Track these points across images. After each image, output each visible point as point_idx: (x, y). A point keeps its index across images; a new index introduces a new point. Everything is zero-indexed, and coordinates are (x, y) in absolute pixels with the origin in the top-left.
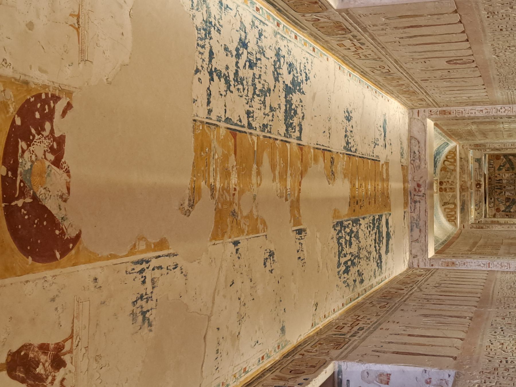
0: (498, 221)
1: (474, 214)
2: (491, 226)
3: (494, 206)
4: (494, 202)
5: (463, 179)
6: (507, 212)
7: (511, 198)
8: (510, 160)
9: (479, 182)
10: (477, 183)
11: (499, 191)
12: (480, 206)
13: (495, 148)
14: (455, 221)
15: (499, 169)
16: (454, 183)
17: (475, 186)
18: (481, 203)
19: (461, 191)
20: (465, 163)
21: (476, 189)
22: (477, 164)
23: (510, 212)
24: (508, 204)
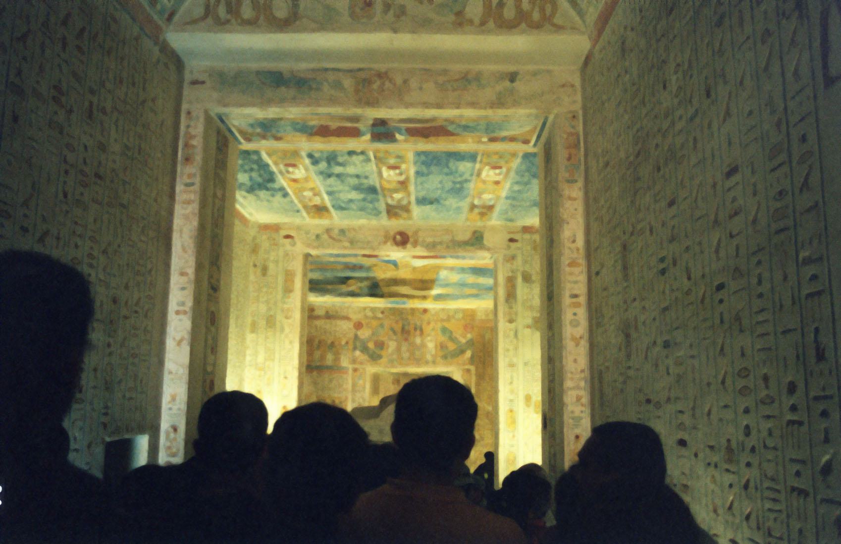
0: (291, 291)
1: (317, 226)
2: (192, 197)
3: (366, 317)
4: (375, 318)
5: (414, 83)
6: (354, 342)
7: (383, 353)
8: (462, 352)
9: (411, 240)
10: (410, 234)
11: (398, 328)
12: (340, 241)
13: (561, 222)
14: (210, 20)
15: (444, 330)
16: (398, 16)
17: (401, 229)
18: (347, 244)
19: (362, 75)
20: (489, 93)
21: (392, 233)
22: (467, 236)
23: (355, 348)
24: (371, 345)
